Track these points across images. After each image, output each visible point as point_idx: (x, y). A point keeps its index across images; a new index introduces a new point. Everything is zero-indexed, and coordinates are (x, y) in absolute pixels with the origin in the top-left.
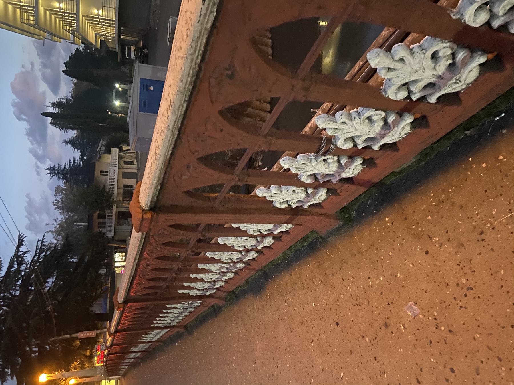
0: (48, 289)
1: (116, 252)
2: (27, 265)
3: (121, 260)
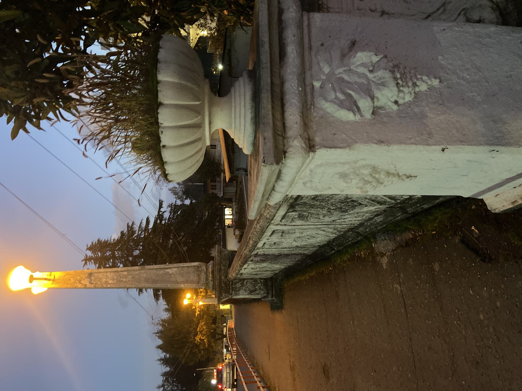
1: (225, 208)
3: (230, 214)
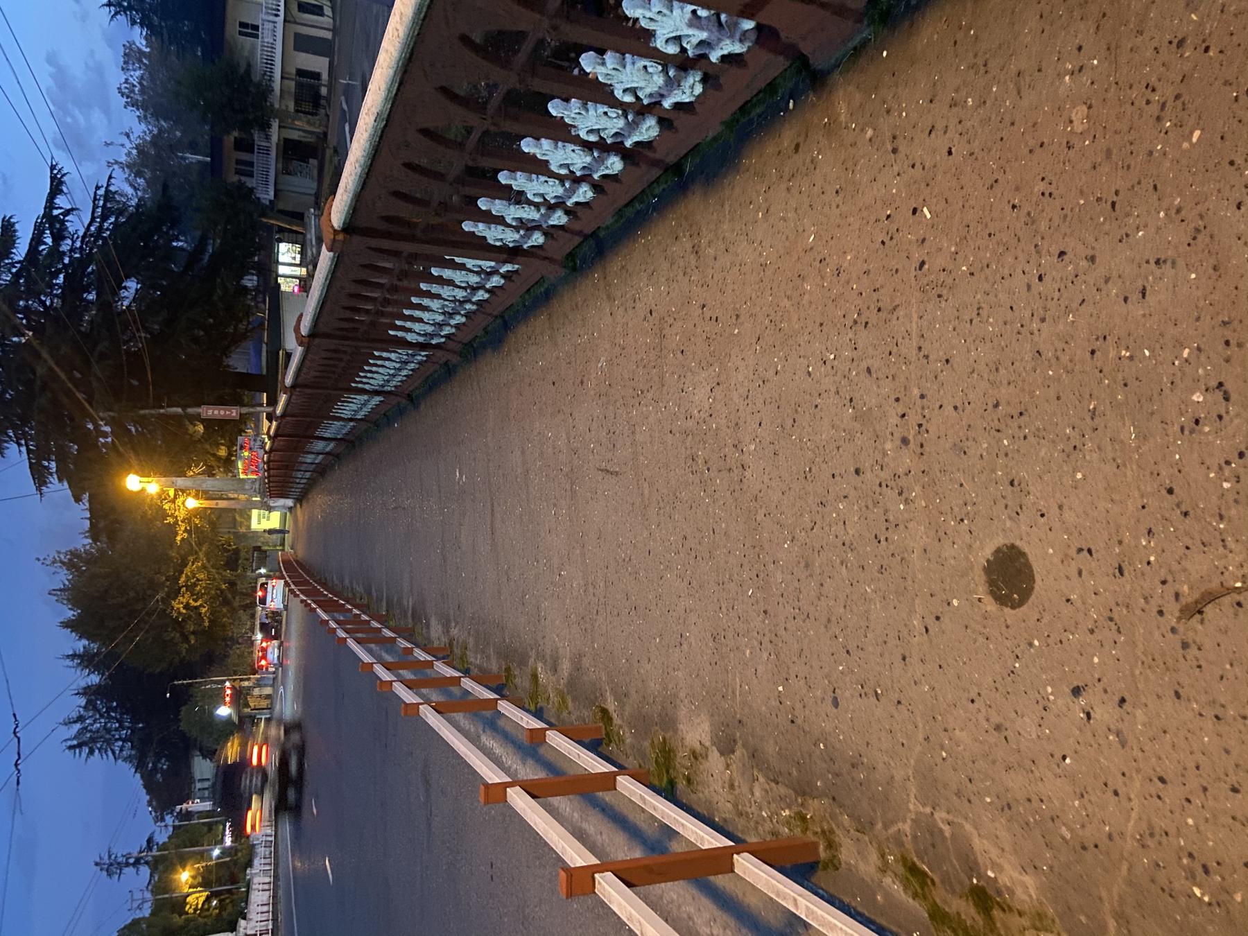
0: (126, 303)
1: (281, 241)
2: (73, 242)
3: (293, 262)
